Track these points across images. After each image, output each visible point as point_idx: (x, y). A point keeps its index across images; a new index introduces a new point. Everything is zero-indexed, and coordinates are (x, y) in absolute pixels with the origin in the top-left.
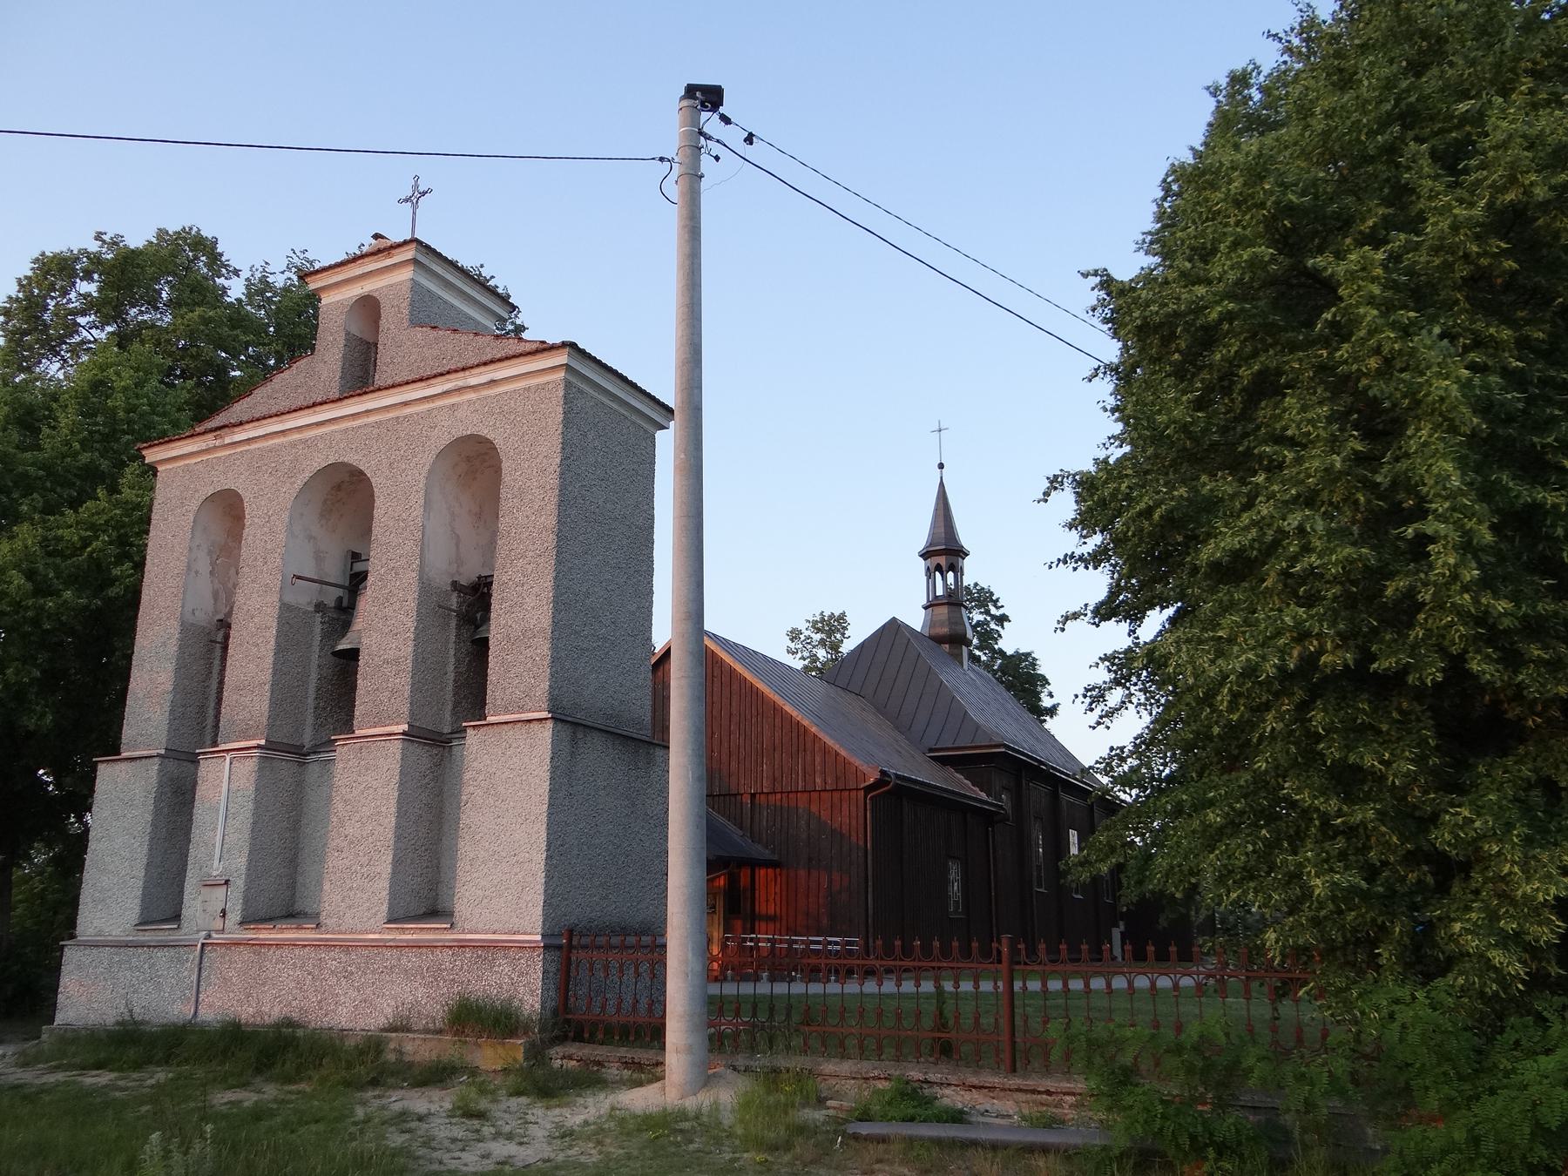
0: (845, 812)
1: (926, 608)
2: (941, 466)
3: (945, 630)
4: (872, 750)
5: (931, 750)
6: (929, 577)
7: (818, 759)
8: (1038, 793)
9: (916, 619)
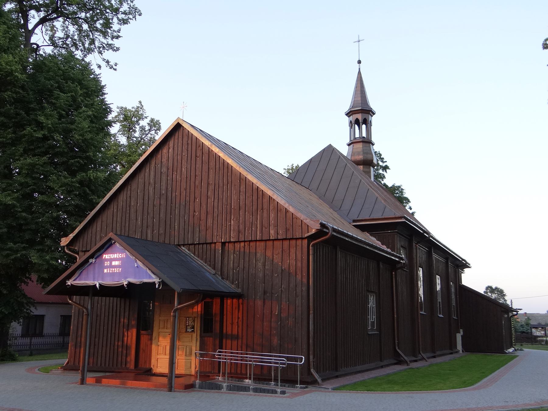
0: (293, 255)
1: (349, 145)
2: (359, 62)
3: (360, 157)
4: (313, 213)
5: (354, 221)
6: (351, 127)
7: (272, 215)
8: (420, 252)
9: (344, 150)
